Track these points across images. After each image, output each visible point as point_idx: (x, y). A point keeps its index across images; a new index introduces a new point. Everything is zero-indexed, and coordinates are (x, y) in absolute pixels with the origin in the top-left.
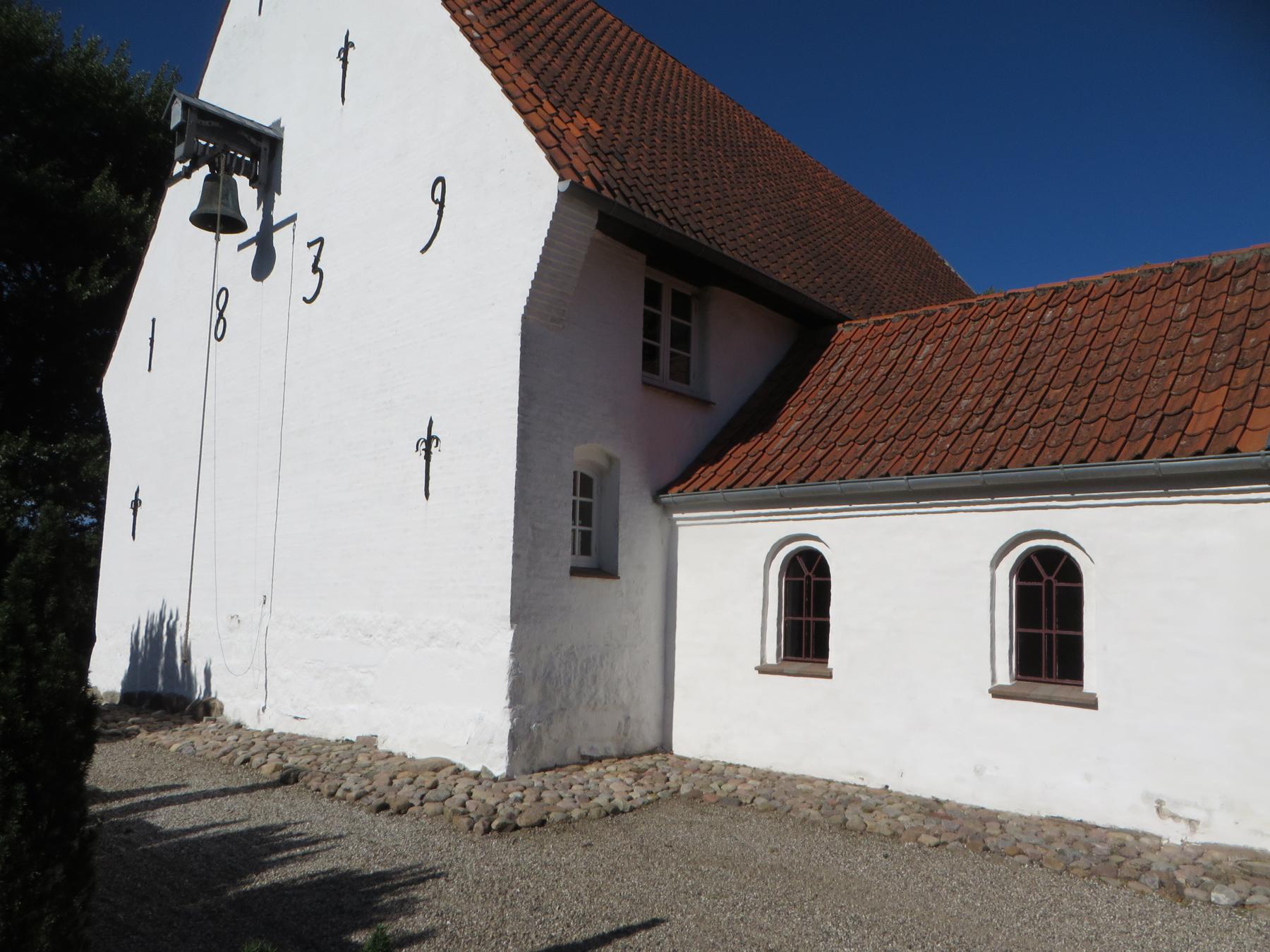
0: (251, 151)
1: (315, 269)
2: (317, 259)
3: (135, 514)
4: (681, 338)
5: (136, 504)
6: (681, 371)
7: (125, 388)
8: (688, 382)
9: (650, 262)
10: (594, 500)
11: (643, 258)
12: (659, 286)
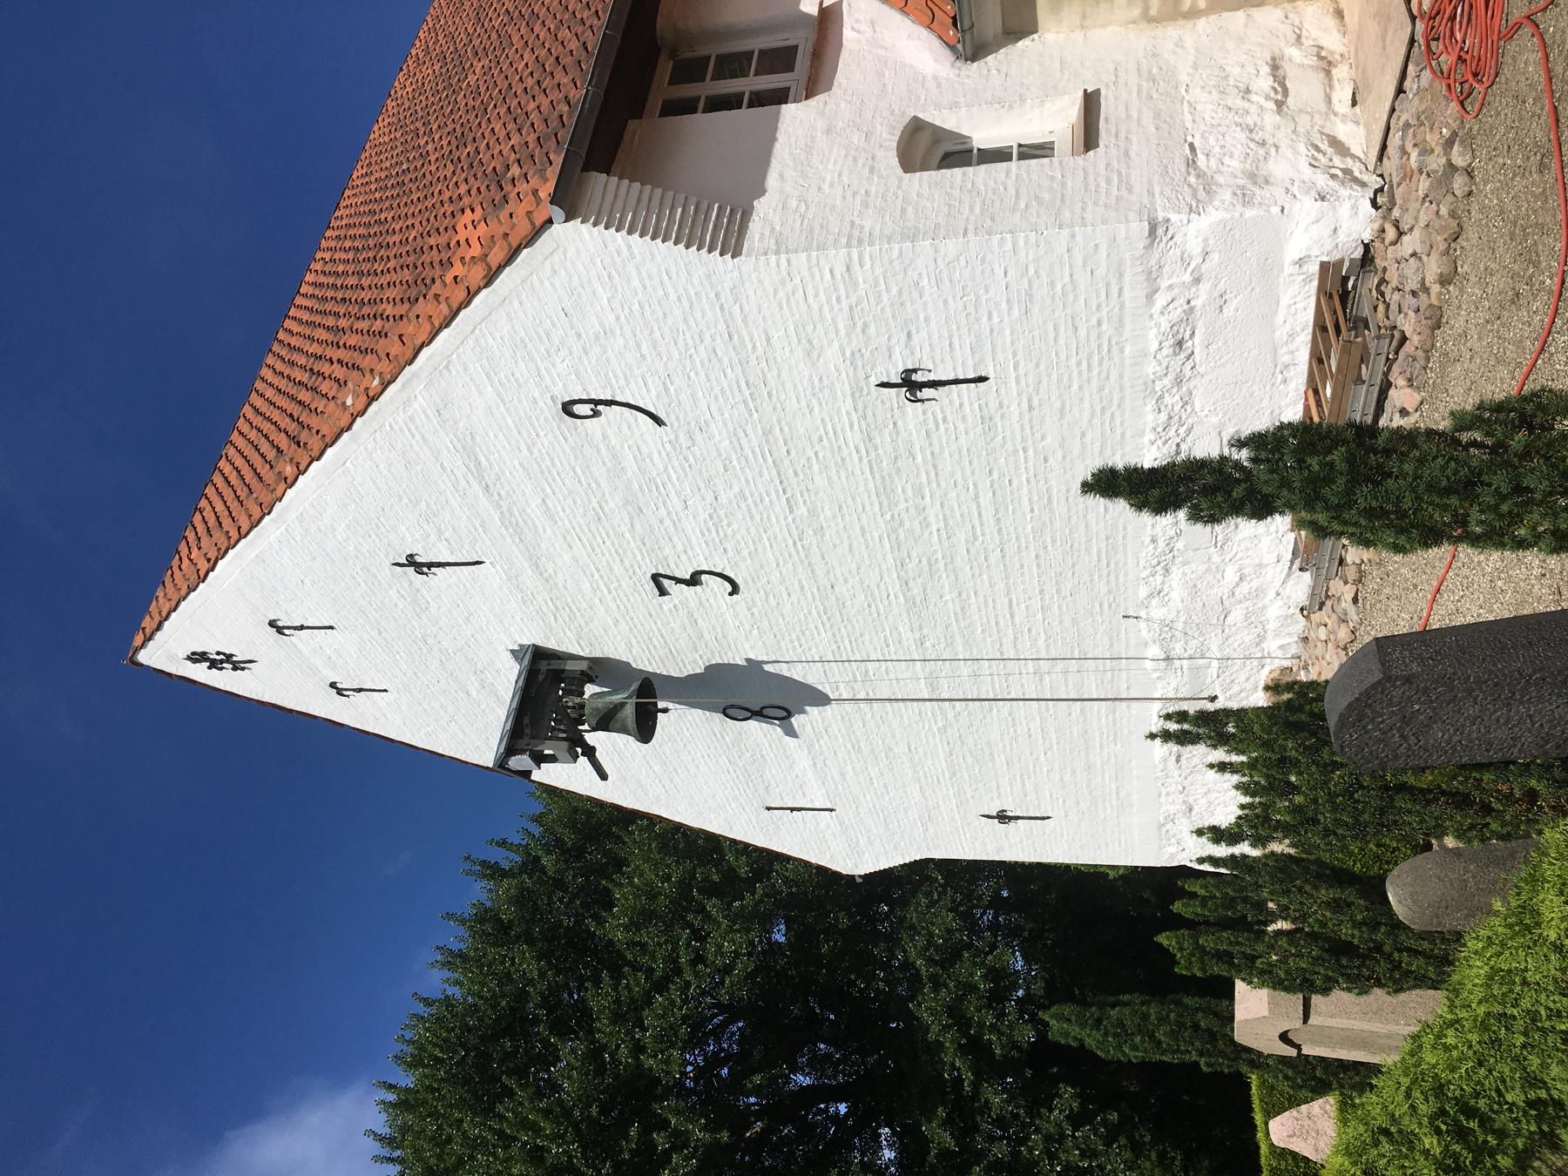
0: (555, 696)
1: (694, 580)
2: (679, 581)
3: (1018, 818)
4: (734, 65)
5: (1003, 817)
6: (781, 59)
7: (856, 848)
8: (671, 83)
9: (638, 113)
10: (1014, 164)
11: (632, 124)
12: (789, 67)
